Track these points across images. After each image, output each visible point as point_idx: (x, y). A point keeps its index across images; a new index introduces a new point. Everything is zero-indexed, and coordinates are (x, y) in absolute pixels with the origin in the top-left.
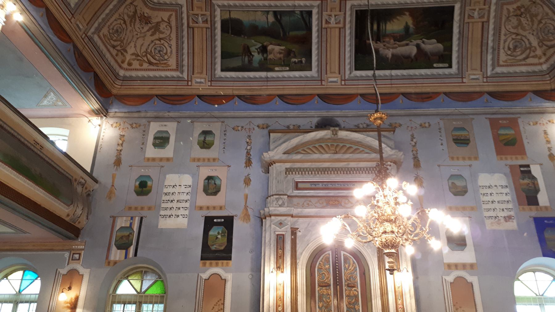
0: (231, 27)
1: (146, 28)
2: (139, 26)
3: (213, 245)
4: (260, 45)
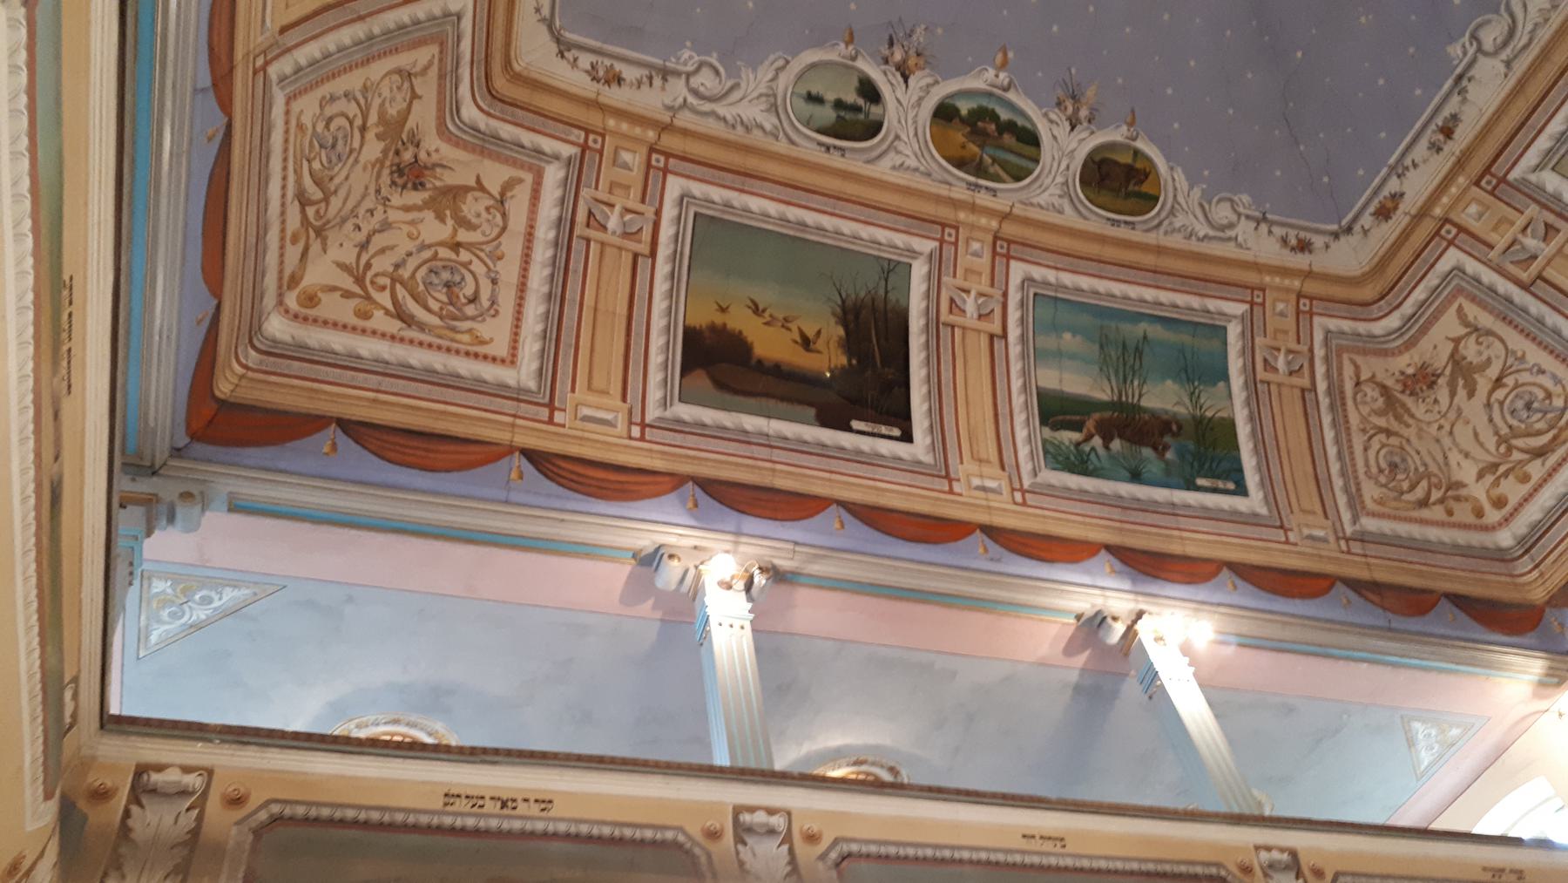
1: (1443, 393)
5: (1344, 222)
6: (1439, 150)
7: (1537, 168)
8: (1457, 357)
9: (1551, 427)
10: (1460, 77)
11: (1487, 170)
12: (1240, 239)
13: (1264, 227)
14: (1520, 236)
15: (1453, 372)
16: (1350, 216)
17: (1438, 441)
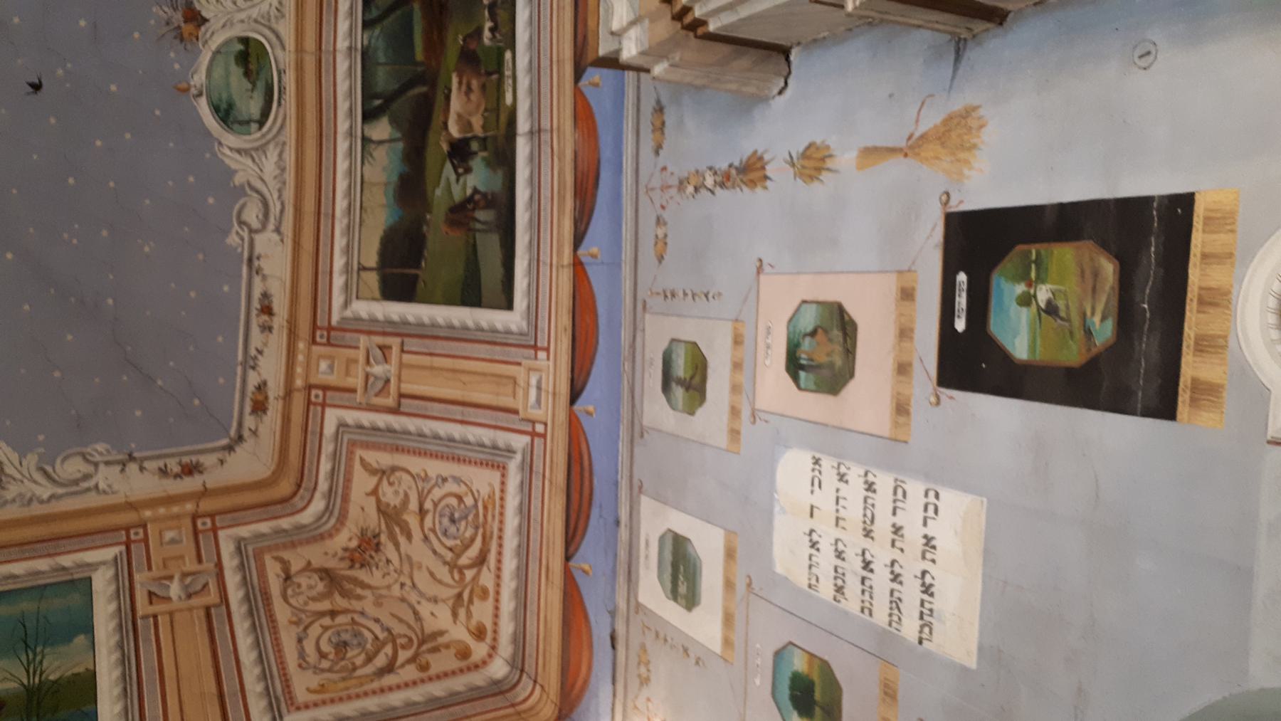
0: (401, 272)
1: (389, 551)
2: (378, 574)
3: (1088, 333)
4: (448, 166)
5: (233, 432)
6: (270, 329)
7: (346, 304)
8: (382, 508)
9: (477, 528)
10: (250, 260)
11: (314, 327)
12: (102, 486)
13: (133, 468)
14: (368, 369)
15: (387, 526)
16: (235, 424)
17: (403, 600)
